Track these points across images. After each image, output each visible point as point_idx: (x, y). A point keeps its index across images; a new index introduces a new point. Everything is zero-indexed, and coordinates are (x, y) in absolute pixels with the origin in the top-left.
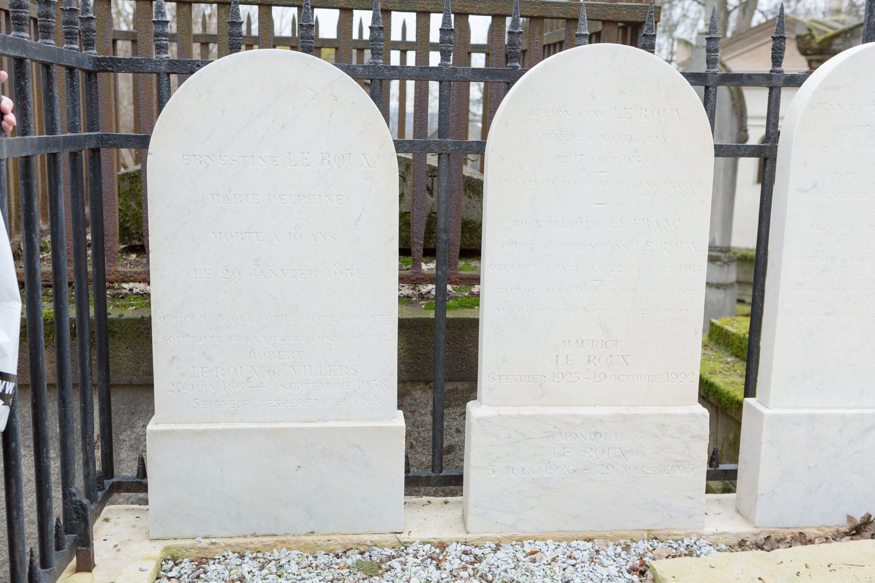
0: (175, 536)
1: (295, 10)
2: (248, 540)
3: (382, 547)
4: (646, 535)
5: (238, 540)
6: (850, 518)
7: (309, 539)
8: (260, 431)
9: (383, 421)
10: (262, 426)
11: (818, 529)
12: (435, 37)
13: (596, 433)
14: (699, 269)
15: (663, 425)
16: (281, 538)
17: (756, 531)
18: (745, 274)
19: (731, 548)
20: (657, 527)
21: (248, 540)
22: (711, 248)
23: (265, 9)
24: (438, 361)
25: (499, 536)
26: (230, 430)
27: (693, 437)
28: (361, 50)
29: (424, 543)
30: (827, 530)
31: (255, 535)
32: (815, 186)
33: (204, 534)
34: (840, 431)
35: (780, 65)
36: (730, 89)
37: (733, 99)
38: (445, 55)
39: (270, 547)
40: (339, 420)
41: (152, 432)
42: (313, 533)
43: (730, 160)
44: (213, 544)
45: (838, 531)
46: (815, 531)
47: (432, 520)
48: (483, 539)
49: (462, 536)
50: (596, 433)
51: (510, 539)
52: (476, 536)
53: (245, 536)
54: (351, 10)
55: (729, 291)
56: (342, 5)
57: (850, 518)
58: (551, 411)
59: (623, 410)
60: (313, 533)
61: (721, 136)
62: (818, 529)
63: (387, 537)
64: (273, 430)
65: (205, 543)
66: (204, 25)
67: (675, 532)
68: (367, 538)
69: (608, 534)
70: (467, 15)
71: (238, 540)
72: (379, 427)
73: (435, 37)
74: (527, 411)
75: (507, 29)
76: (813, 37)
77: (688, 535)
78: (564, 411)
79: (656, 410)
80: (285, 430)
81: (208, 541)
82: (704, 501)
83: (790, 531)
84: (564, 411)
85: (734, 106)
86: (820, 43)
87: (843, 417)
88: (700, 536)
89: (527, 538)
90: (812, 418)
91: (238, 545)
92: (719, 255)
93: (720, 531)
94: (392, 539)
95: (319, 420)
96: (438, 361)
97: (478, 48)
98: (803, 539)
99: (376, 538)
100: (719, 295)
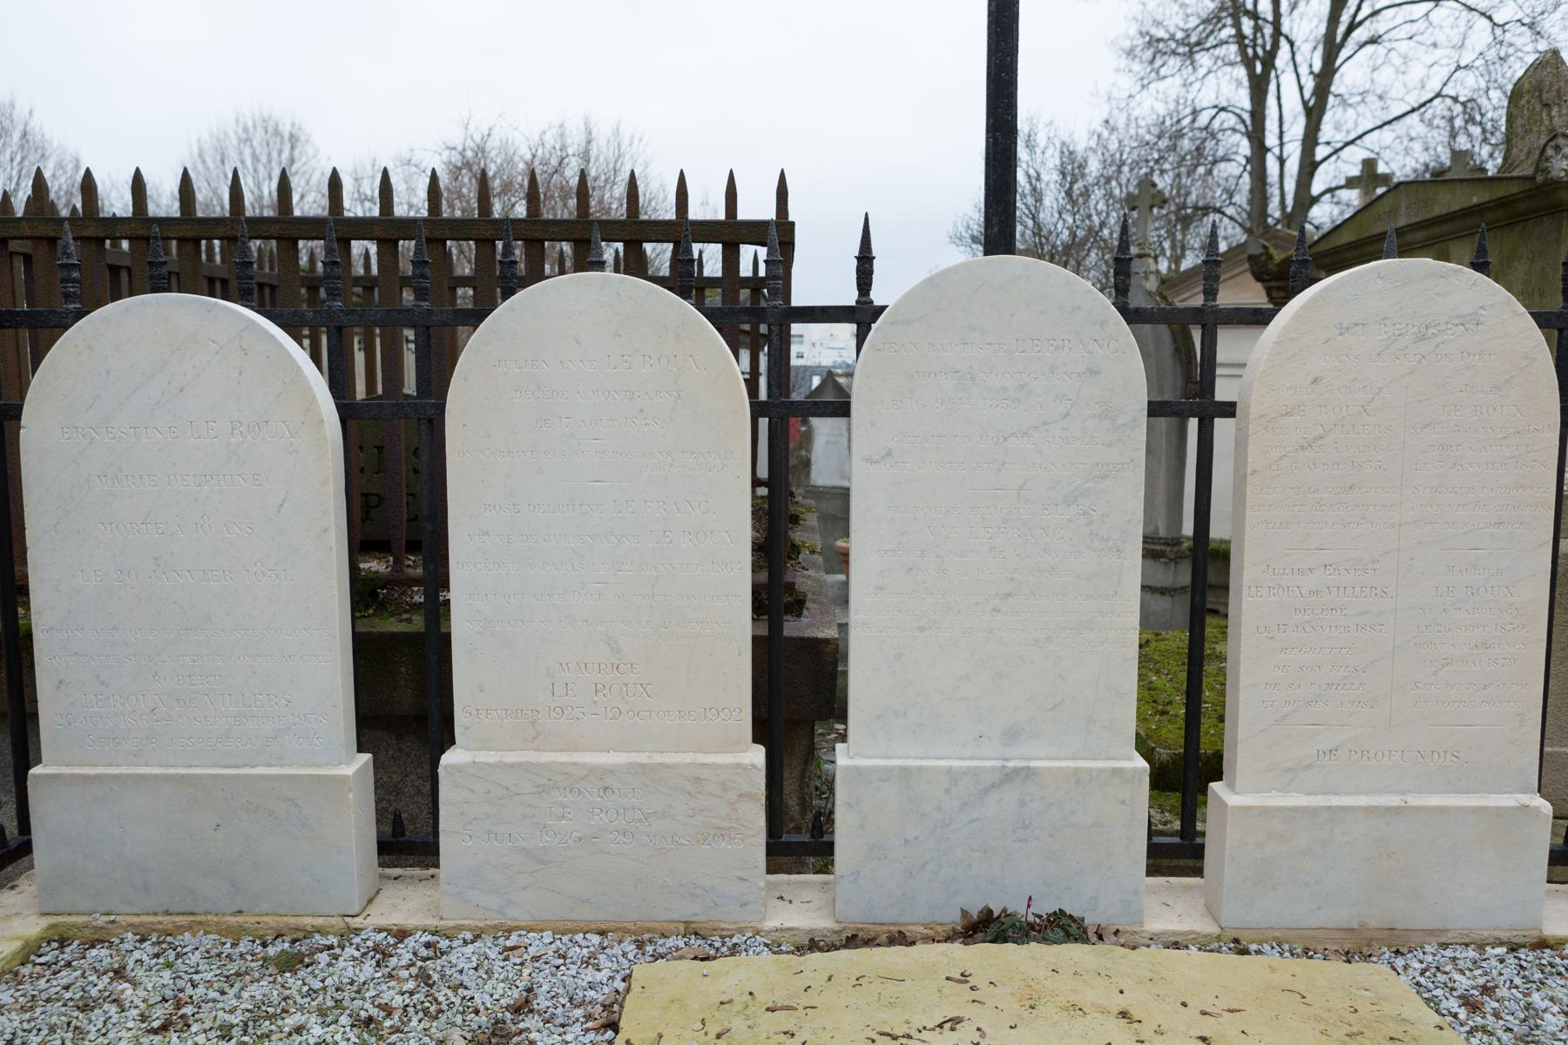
0: (69, 909)
1: (620, 246)
2: (159, 918)
3: (327, 933)
4: (682, 929)
5: (144, 919)
6: (964, 913)
7: (232, 920)
8: (166, 777)
9: (341, 766)
10: (171, 771)
11: (926, 926)
12: (407, 268)
13: (606, 789)
14: (1131, 569)
15: (698, 780)
16: (199, 918)
17: (837, 927)
18: (1192, 579)
19: (800, 950)
20: (698, 918)
21: (159, 918)
22: (1147, 539)
23: (189, 247)
24: (403, 692)
25: (481, 924)
26: (129, 776)
27: (740, 796)
28: (313, 289)
29: (380, 931)
30: (939, 929)
31: (167, 913)
32: (889, 454)
33: (103, 909)
34: (947, 791)
35: (1214, 300)
36: (1170, 328)
37: (1175, 341)
38: (421, 294)
39: (180, 929)
40: (270, 765)
41: (34, 776)
42: (240, 912)
43: (1174, 420)
44: (113, 922)
45: (954, 930)
46: (921, 929)
47: (406, 904)
48: (460, 928)
49: (432, 922)
50: (606, 789)
51: (496, 928)
52: (451, 923)
53: (156, 914)
54: (396, 242)
55: (1177, 598)
56: (727, 239)
57: (964, 913)
58: (545, 757)
59: (642, 758)
60: (240, 912)
61: (1161, 390)
62: (926, 926)
63: (333, 921)
64: (183, 776)
65: (102, 920)
66: (367, 265)
67: (723, 926)
68: (308, 921)
69: (630, 926)
70: (641, 243)
71: (144, 919)
72: (318, 776)
73: (407, 268)
74: (511, 758)
75: (498, 257)
76: (1270, 257)
77: (741, 931)
78: (563, 758)
79: (689, 758)
80: (199, 777)
81: (106, 918)
82: (762, 884)
83: (885, 928)
84: (563, 758)
85: (1176, 349)
86: (1278, 265)
87: (949, 770)
88: (757, 932)
89: (518, 928)
90: (906, 771)
91: (141, 925)
92: (1155, 549)
93: (787, 925)
94: (337, 922)
95: (246, 765)
96: (403, 692)
97: (464, 281)
98: (900, 939)
99: (320, 921)
100: (1162, 604)
